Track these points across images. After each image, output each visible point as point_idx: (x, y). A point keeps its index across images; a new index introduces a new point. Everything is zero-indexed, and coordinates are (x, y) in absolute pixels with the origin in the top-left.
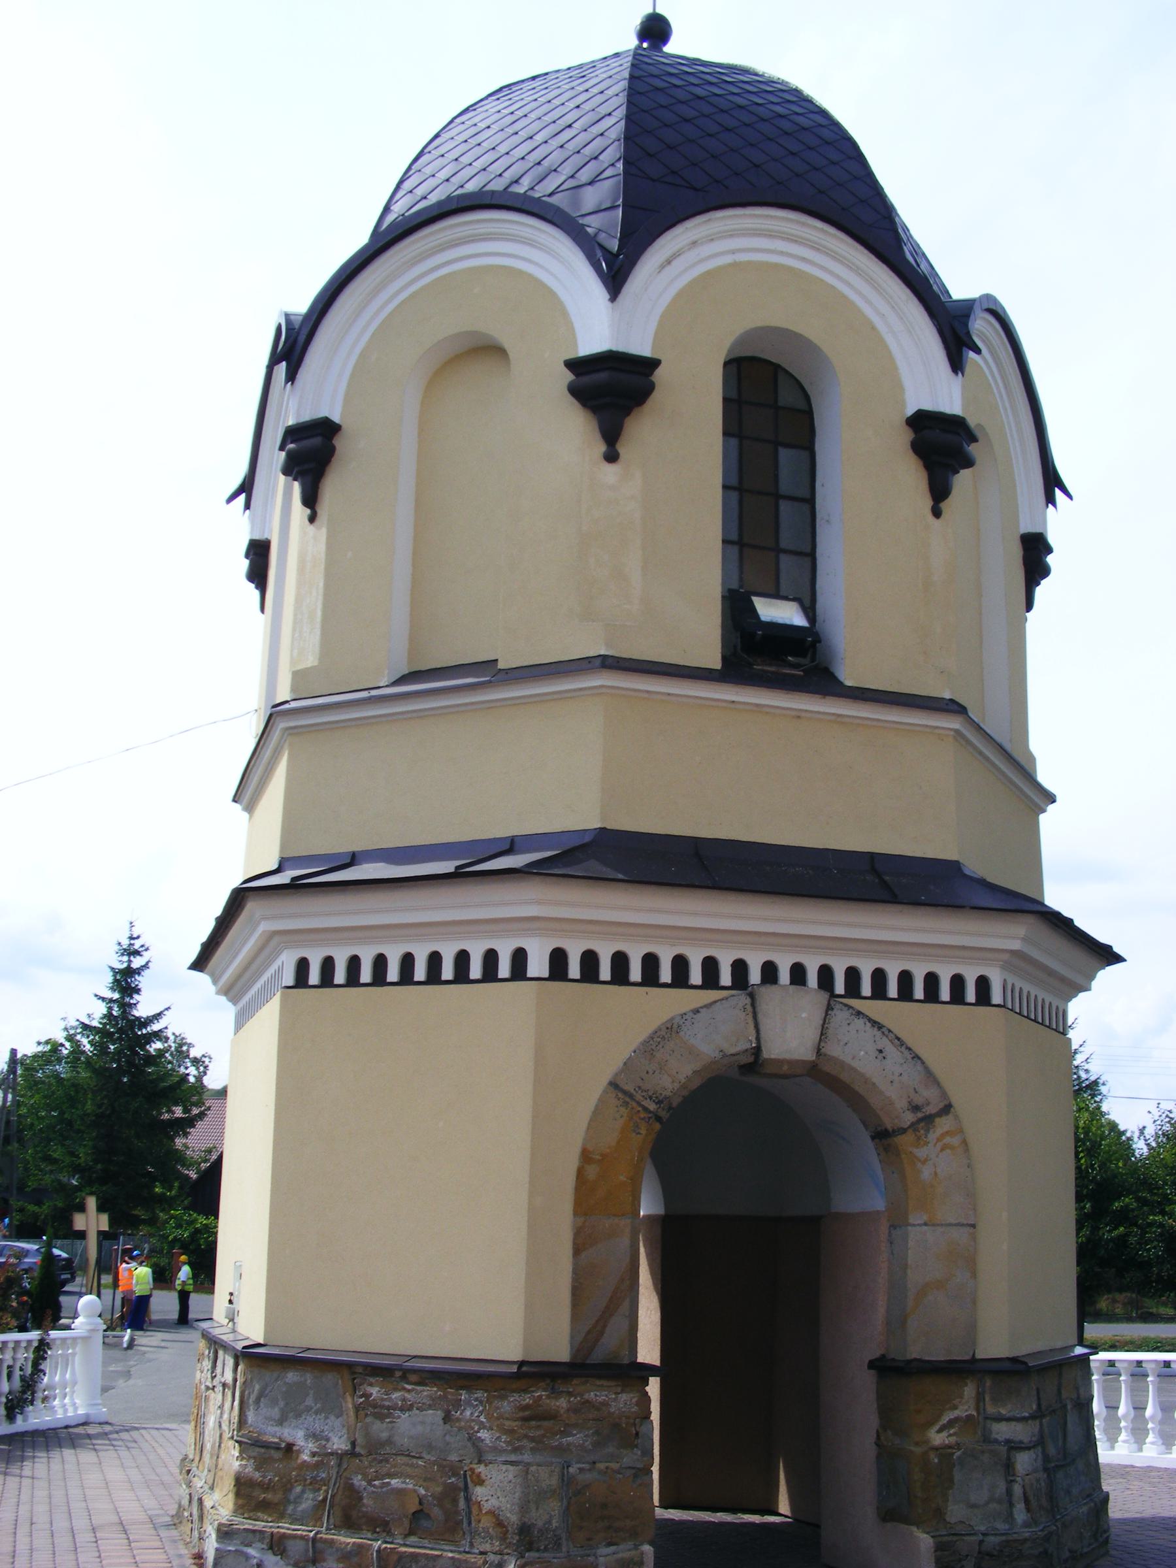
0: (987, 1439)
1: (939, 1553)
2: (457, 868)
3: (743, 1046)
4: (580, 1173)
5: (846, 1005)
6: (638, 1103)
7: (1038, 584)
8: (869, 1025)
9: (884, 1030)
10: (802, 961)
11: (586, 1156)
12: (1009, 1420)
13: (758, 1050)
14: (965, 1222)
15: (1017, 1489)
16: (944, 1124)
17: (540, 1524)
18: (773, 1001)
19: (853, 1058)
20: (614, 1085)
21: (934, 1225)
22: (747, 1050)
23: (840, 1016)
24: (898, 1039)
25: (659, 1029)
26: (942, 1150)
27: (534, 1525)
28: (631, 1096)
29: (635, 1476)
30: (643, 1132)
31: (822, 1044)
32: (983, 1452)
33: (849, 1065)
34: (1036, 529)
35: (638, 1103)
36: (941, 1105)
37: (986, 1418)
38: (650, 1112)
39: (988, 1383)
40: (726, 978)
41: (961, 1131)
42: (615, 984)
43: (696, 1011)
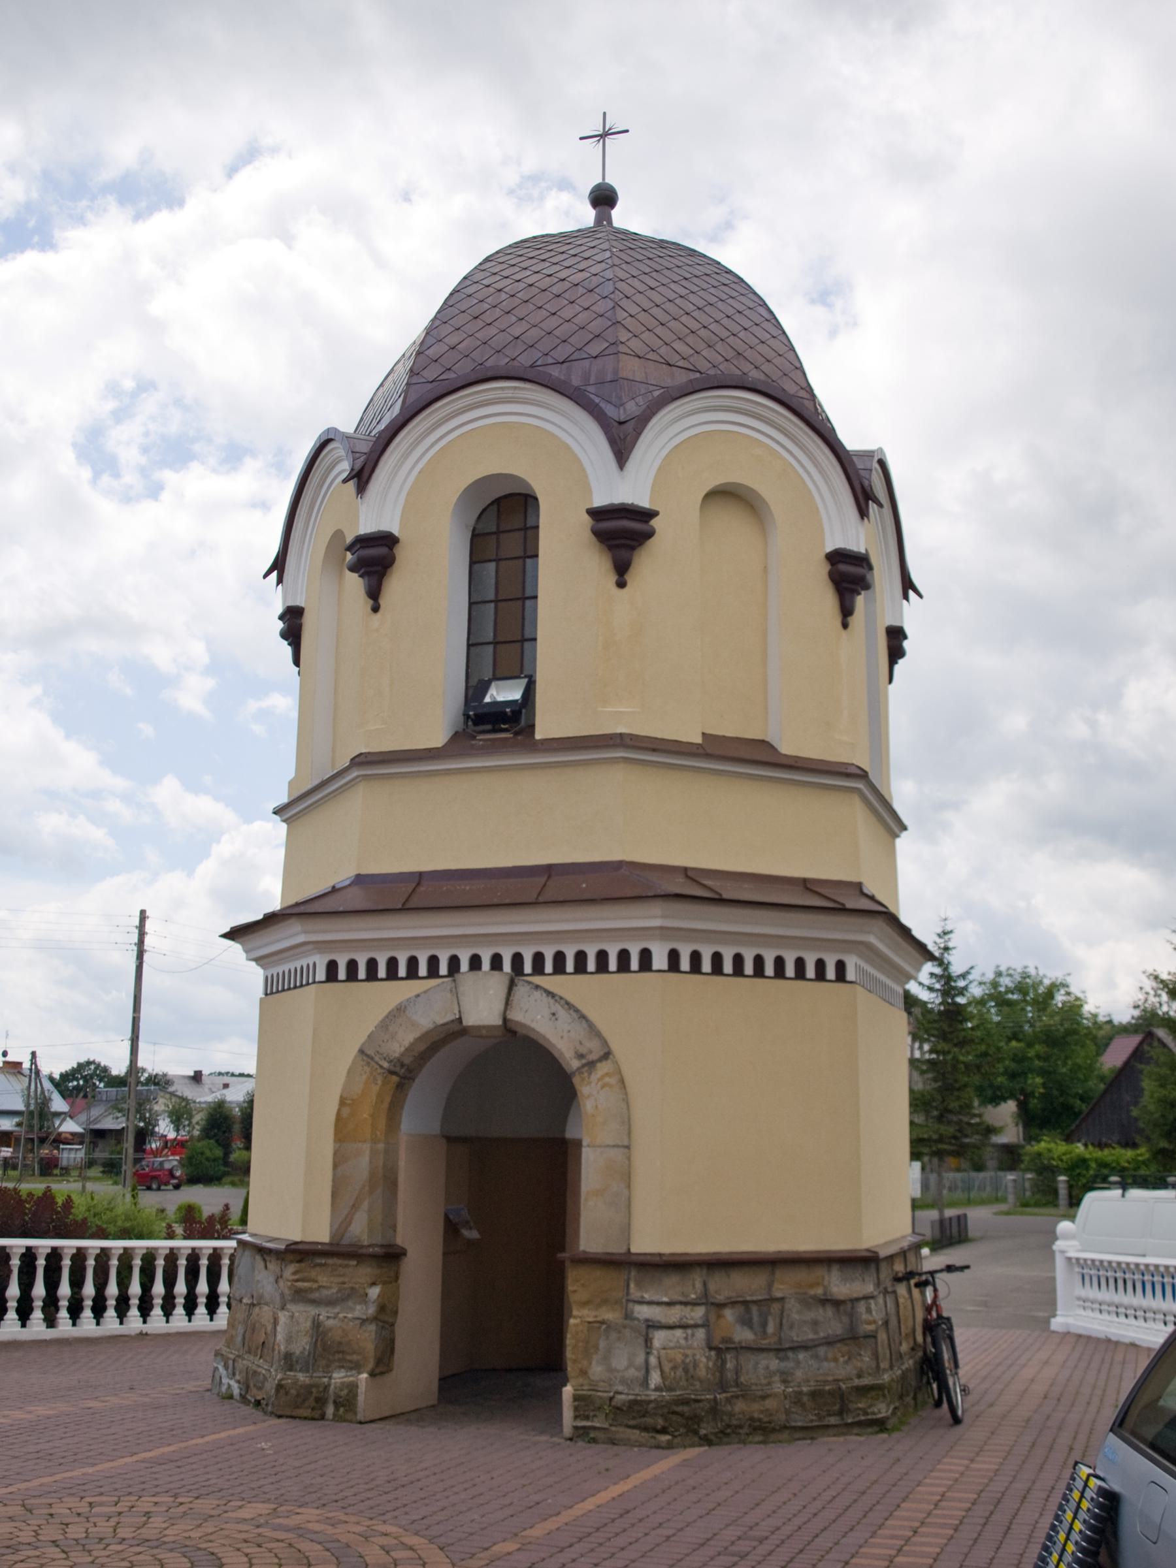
0: (628, 1316)
1: (576, 1403)
3: (450, 1017)
4: (338, 1114)
6: (377, 1063)
7: (897, 663)
8: (544, 995)
9: (557, 998)
11: (343, 1102)
12: (650, 1303)
13: (460, 1020)
15: (653, 1360)
16: (603, 1068)
17: (298, 1352)
19: (532, 1021)
20: (361, 1051)
21: (593, 1146)
22: (453, 1021)
23: (521, 990)
24: (567, 1003)
25: (393, 1010)
26: (602, 1087)
27: (294, 1353)
28: (372, 1058)
30: (379, 1082)
31: (508, 1012)
32: (625, 1327)
34: (896, 623)
35: (377, 1063)
36: (602, 1053)
37: (628, 1301)
40: (443, 969)
41: (620, 1072)
43: (418, 996)
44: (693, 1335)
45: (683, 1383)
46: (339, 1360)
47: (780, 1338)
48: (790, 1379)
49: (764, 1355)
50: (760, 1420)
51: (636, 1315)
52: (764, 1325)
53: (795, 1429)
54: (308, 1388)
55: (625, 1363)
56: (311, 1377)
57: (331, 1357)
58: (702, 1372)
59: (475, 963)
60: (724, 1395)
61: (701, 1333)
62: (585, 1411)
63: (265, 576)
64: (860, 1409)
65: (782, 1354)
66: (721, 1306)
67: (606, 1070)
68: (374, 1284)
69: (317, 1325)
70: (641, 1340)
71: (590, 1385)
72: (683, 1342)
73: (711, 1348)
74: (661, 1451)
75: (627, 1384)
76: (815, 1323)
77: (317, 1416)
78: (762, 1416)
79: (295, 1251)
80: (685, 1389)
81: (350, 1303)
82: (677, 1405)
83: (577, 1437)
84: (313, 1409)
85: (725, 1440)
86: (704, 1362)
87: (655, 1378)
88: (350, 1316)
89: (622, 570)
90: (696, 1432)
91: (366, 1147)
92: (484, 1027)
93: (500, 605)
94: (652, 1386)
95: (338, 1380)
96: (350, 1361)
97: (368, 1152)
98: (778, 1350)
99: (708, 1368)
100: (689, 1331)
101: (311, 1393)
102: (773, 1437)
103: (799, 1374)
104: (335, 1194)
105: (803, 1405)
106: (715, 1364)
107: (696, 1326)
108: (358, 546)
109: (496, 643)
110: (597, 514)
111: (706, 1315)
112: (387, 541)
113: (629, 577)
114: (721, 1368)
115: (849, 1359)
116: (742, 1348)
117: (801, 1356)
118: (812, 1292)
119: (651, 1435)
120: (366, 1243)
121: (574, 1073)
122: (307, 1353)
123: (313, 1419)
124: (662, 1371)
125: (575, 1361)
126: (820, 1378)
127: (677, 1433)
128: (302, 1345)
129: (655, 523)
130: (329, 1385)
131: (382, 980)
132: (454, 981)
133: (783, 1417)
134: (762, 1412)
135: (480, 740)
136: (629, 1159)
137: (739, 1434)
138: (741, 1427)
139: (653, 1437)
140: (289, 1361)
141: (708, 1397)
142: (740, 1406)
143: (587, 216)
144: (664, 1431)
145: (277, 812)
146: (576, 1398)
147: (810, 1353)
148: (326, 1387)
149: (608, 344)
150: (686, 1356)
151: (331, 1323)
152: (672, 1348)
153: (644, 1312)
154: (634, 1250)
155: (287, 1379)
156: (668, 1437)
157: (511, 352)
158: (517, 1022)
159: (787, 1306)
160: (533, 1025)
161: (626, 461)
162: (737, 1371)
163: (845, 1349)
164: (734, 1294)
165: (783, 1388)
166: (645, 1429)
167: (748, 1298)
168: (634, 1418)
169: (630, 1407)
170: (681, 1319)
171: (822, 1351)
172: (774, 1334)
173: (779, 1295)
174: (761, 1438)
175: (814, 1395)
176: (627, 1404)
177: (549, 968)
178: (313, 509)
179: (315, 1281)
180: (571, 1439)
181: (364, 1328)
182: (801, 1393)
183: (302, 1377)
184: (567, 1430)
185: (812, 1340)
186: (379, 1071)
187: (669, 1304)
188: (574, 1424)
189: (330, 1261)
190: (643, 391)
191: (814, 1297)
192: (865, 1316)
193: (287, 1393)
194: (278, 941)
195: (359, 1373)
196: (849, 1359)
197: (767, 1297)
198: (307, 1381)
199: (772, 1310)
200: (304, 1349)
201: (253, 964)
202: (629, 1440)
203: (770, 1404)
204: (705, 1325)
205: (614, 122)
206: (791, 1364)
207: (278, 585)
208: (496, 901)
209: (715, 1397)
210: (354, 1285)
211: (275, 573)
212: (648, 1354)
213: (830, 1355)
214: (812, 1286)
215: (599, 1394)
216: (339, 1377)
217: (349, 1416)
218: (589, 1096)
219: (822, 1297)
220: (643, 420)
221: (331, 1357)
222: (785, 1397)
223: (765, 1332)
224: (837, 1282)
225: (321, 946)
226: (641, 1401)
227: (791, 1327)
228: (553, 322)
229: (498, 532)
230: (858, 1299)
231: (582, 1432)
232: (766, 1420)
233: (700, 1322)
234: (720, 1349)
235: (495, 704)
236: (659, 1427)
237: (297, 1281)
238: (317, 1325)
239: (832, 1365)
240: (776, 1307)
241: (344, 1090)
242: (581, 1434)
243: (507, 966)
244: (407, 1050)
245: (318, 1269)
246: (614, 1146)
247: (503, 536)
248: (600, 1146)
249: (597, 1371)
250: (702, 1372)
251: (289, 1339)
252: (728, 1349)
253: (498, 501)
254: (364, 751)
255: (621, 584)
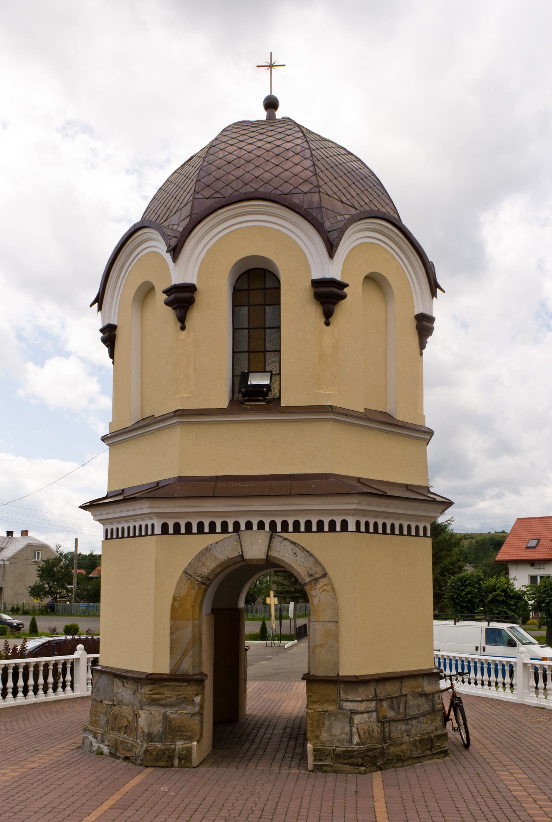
0: (341, 708)
1: (315, 753)
2: (124, 497)
5: (280, 536)
8: (289, 543)
9: (296, 545)
10: (179, 522)
11: (175, 599)
12: (351, 701)
13: (242, 556)
14: (333, 621)
15: (354, 730)
16: (323, 582)
17: (155, 732)
18: (246, 536)
19: (283, 557)
20: (185, 572)
22: (238, 556)
23: (277, 540)
24: (303, 548)
25: (203, 550)
26: (322, 592)
28: (191, 576)
29: (192, 716)
30: (196, 589)
31: (269, 552)
32: (339, 714)
33: (282, 560)
35: (194, 578)
36: (322, 574)
37: (340, 700)
38: (199, 581)
39: (342, 686)
40: (231, 529)
41: (331, 583)
42: (187, 534)
43: (217, 543)
44: (371, 716)
45: (369, 740)
46: (180, 735)
47: (405, 714)
48: (410, 734)
49: (399, 723)
50: (400, 755)
51: (344, 707)
52: (399, 708)
53: (414, 758)
54: (163, 751)
55: (339, 732)
56: (165, 745)
57: (175, 734)
58: (376, 734)
59: (249, 525)
60: (386, 744)
61: (374, 715)
62: (319, 757)
63: (91, 306)
64: (438, 746)
65: (406, 722)
66: (382, 700)
67: (324, 583)
68: (197, 695)
69: (165, 717)
70: (347, 720)
71: (321, 743)
72: (367, 720)
73: (379, 722)
74: (362, 775)
75: (341, 742)
76: (418, 706)
77: (169, 765)
78: (401, 753)
79: (150, 679)
80: (369, 744)
81: (184, 706)
82: (368, 752)
83: (316, 770)
84: (167, 762)
85: (387, 767)
86: (376, 728)
87: (356, 739)
88: (184, 712)
89: (328, 315)
90: (375, 764)
91: (190, 623)
92: (256, 560)
93: (251, 331)
94: (355, 743)
95: (180, 746)
96: (186, 736)
97: (191, 626)
98: (404, 720)
99: (378, 732)
100: (370, 714)
101: (165, 753)
102: (406, 763)
103: (413, 731)
104: (172, 648)
105: (417, 747)
106: (381, 729)
107: (372, 711)
108: (174, 291)
109: (249, 352)
110: (316, 283)
111: (376, 706)
112: (191, 288)
113: (331, 320)
114: (383, 731)
115: (432, 722)
116: (391, 720)
117: (414, 722)
118: (417, 691)
119: (356, 767)
120: (191, 673)
121: (306, 584)
122: (161, 732)
123: (167, 767)
124: (359, 735)
125: (312, 732)
126: (421, 732)
127: (367, 766)
128: (157, 728)
129: (346, 290)
130: (175, 749)
131: (195, 534)
132: (239, 535)
133: (409, 753)
134: (400, 751)
135: (248, 405)
136: (338, 628)
137: (392, 763)
138: (393, 760)
139: (356, 769)
140: (150, 737)
141: (379, 746)
142: (392, 750)
143: (262, 115)
144: (362, 765)
145: (104, 439)
146: (315, 750)
147: (417, 720)
148: (174, 750)
149: (313, 186)
150: (369, 727)
151: (173, 716)
152: (363, 724)
153: (348, 706)
154: (340, 674)
155: (150, 747)
156: (364, 768)
157: (255, 186)
158: (274, 557)
159: (408, 698)
160: (284, 559)
161: (179, 254)
162: (390, 732)
163: (430, 717)
164: (387, 694)
165: (408, 739)
166: (352, 764)
167: (393, 696)
168: (346, 759)
169: (344, 754)
170: (366, 708)
171: (421, 719)
172: (403, 712)
173: (405, 693)
174: (401, 764)
175: (421, 741)
176: (342, 753)
177: (291, 529)
178: (123, 268)
179: (162, 694)
180: (312, 771)
181: (193, 718)
182: (416, 740)
183: (159, 745)
184: (310, 766)
185: (418, 714)
186: (196, 582)
187: (361, 701)
188: (314, 764)
189: (172, 684)
190: (332, 216)
191: (417, 693)
192: (437, 701)
193: (151, 754)
194: (125, 511)
195: (192, 742)
196: (432, 722)
197: (400, 695)
198: (163, 747)
199: (402, 701)
200: (159, 730)
201: (98, 522)
202: (344, 770)
203: (404, 747)
204: (376, 710)
205: (277, 60)
206: (410, 727)
207: (98, 311)
208: (266, 493)
209: (383, 746)
210: (186, 696)
211: (97, 304)
212: (351, 727)
213: (424, 721)
214: (417, 687)
215: (327, 748)
216: (180, 744)
217: (187, 764)
218: (315, 596)
219: (421, 693)
220: (342, 231)
221: (175, 734)
222: (410, 743)
223: (399, 712)
224: (427, 685)
225: (158, 515)
226: (350, 751)
227: (409, 708)
228: (278, 170)
229: (248, 290)
230: (435, 693)
231: (319, 767)
232: (403, 755)
233: (374, 709)
234: (383, 721)
235: (251, 385)
236: (360, 763)
237: (152, 694)
238: (165, 717)
239: (426, 725)
240: (403, 699)
241: (175, 593)
242: (318, 768)
243: (267, 528)
244: (212, 571)
245: (164, 688)
246: (329, 622)
247: (251, 292)
248: (322, 622)
249: (324, 736)
250: (376, 734)
251: (150, 726)
252: (386, 721)
253: (248, 272)
254: (180, 408)
255: (327, 324)
